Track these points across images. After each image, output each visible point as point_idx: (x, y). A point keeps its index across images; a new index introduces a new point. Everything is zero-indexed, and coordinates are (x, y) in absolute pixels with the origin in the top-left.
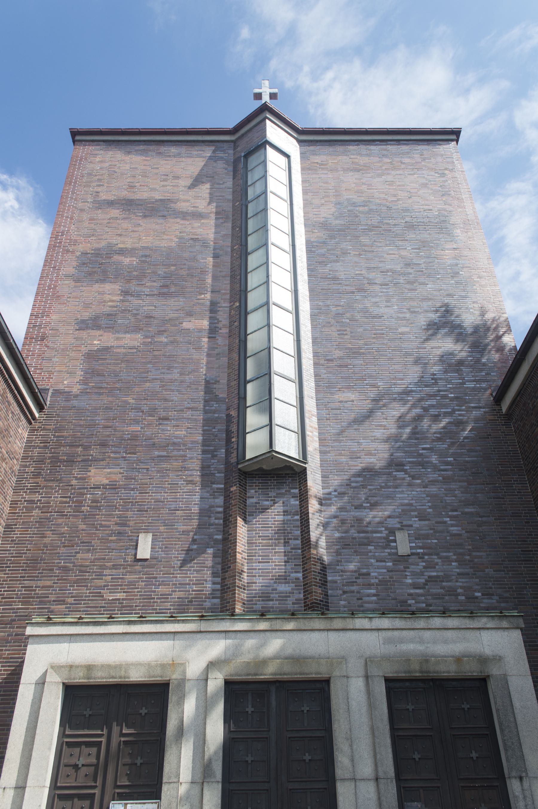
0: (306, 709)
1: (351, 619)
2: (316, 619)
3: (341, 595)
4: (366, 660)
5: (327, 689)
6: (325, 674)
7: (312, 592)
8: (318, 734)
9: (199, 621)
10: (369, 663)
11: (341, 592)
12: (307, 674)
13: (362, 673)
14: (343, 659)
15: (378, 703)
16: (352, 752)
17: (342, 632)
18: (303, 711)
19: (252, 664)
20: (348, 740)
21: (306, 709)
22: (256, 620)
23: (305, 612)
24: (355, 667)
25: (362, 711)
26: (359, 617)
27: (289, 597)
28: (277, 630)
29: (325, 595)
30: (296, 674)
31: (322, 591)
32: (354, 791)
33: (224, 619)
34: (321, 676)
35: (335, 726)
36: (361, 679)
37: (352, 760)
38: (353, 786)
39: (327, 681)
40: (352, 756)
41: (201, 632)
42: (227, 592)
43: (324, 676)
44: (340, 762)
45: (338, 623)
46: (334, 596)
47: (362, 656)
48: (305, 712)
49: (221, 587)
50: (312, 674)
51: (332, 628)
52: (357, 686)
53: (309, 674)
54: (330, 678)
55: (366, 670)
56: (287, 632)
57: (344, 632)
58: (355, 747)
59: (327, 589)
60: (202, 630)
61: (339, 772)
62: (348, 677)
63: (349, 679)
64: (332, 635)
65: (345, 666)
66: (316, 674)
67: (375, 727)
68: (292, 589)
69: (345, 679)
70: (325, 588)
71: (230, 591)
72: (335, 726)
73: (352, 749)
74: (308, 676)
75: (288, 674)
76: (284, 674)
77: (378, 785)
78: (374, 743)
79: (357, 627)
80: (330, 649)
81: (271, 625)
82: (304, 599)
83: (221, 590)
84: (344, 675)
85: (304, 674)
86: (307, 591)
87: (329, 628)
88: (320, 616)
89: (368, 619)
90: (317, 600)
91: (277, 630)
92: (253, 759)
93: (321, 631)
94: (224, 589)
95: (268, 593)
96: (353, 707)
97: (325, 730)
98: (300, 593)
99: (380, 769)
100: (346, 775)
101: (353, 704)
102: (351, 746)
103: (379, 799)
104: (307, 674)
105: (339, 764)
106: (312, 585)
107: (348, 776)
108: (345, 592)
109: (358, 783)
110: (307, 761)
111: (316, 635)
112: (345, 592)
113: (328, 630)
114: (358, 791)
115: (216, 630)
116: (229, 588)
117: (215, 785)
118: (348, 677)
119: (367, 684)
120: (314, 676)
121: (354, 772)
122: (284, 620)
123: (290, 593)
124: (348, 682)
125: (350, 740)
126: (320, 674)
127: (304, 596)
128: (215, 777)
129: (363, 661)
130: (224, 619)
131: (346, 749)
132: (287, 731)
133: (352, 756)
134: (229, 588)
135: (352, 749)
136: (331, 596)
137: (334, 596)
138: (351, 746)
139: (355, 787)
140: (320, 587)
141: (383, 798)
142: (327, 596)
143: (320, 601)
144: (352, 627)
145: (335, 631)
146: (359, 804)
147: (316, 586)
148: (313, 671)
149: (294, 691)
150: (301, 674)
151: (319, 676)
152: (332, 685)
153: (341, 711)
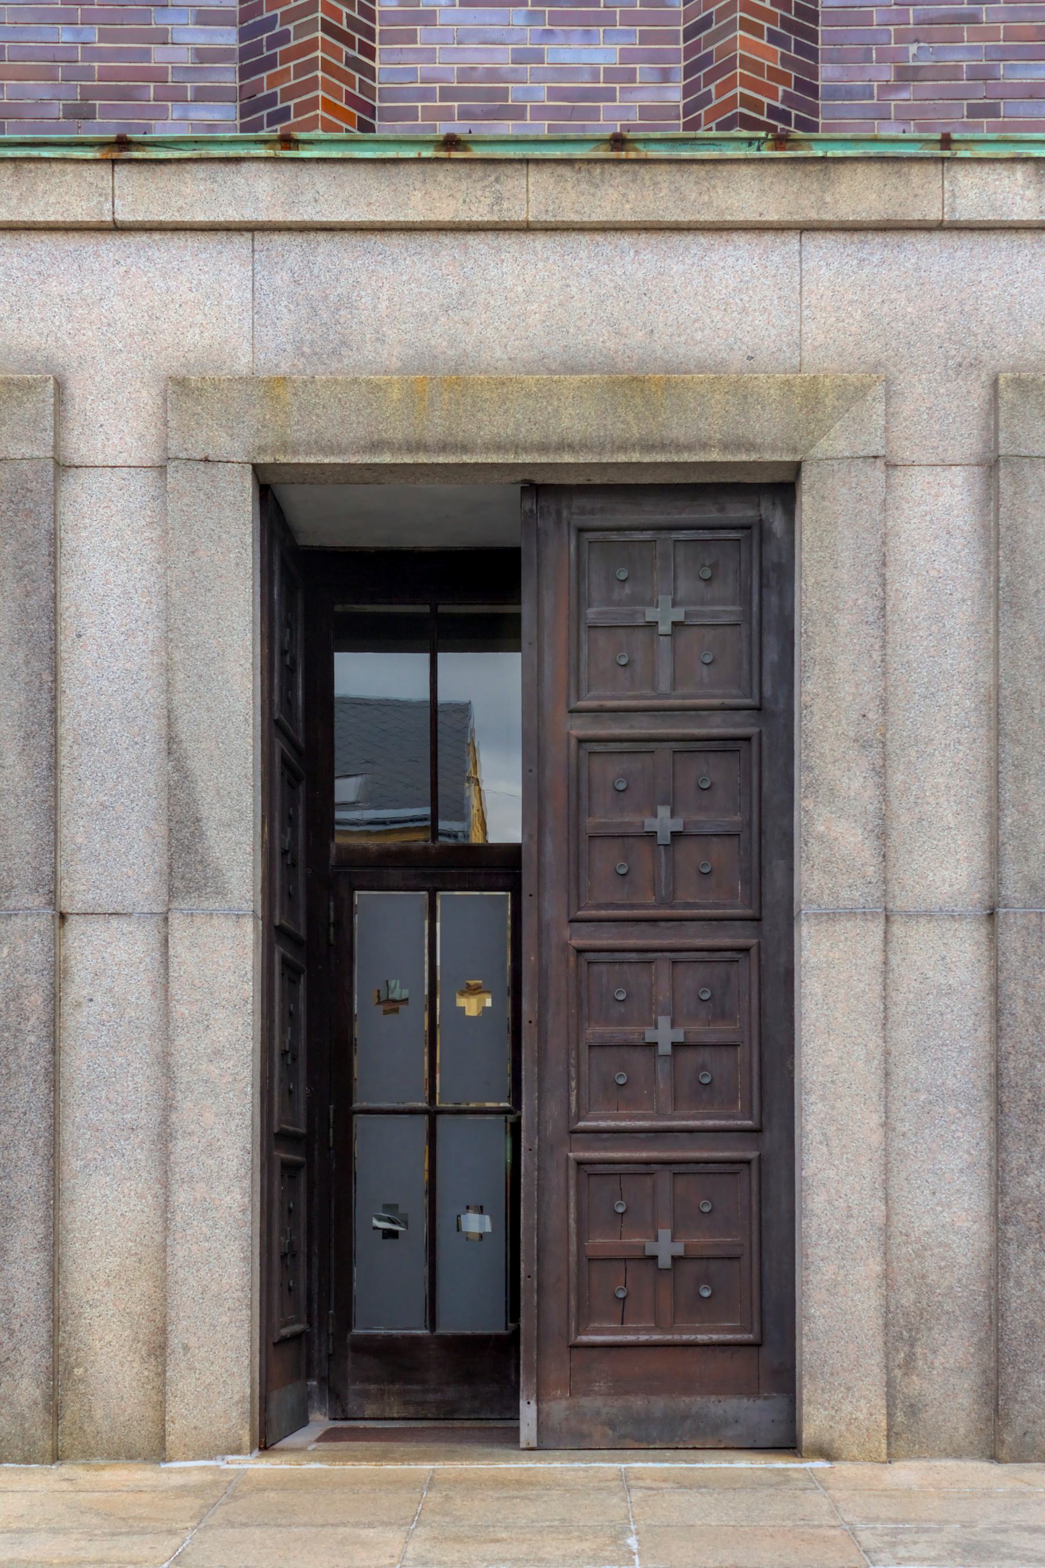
0: (664, 615)
1: (933, 169)
2: (745, 170)
3: (886, 88)
4: (995, 382)
5: (778, 524)
6: (774, 449)
7: (730, 65)
8: (717, 727)
9: (104, 170)
10: (1007, 395)
11: (888, 74)
12: (679, 448)
13: (966, 441)
14: (869, 384)
15: (1032, 585)
16: (885, 799)
17: (878, 239)
18: (653, 625)
19: (395, 394)
20: (865, 745)
21: (664, 615)
22: (414, 169)
23: (691, 134)
24: (940, 417)
25: (949, 623)
26: (980, 161)
27: (609, 95)
28: (527, 228)
29: (800, 84)
30: (623, 448)
31: (785, 60)
32: (879, 957)
33: (238, 160)
34: (753, 457)
35: (809, 686)
36: (959, 476)
37: (882, 835)
38: (877, 939)
39: (782, 488)
40: (883, 818)
41: (117, 228)
42: (270, 63)
43: (768, 457)
44: (821, 838)
45: (860, 194)
46: (850, 94)
47: (976, 364)
48: (665, 628)
49: (243, 36)
50: (705, 446)
51: (828, 217)
52: (938, 506)
53: (689, 448)
54: (797, 468)
55: (992, 430)
56: (585, 239)
57: (892, 238)
58: (898, 779)
59: (813, 54)
60: (124, 216)
61: (812, 881)
62: (891, 466)
63: (899, 473)
64: (825, 257)
65: (881, 407)
66: (725, 447)
67: (1005, 693)
68: (626, 56)
69: (878, 473)
70: (800, 48)
71: (288, 56)
72: (809, 688)
73: (883, 788)
74: (686, 457)
75: (585, 446)
76: (563, 446)
77: (993, 938)
78: (996, 762)
79: (965, 213)
80: (809, 327)
81: (499, 199)
82: (688, 109)
83: (244, 53)
84: (871, 450)
85: (663, 447)
86: (707, 59)
87: (813, 215)
88: (766, 153)
89: (1030, 167)
90: (757, 106)
91: (527, 228)
92: (681, 1039)
93: (768, 238)
94: (256, 49)
95: (493, 74)
96: (906, 605)
97: (759, 709)
98: (665, 76)
99: (1010, 871)
100: (845, 894)
101: (909, 591)
102: (881, 772)
103: (996, 989)
104: (679, 448)
105: (815, 848)
106: (730, 27)
107: (852, 895)
108: (906, 75)
109: (897, 929)
110: (664, 838)
111: (737, 257)
112: (906, 75)
113: (805, 228)
114: (895, 960)
115: (201, 217)
116: (284, 37)
117: (225, 927)
118: (891, 466)
119: (990, 497)
120: (715, 456)
121: (885, 882)
122: (565, 171)
123: (611, 74)
124: (889, 487)
125: (881, 754)
126: (751, 447)
127: (687, 91)
128: (221, 892)
129: (978, 396)
130: (238, 160)
131: (856, 785)
132: (571, 712)
133: (883, 818)
134: (284, 37)
135: (883, 788)
136: (834, 93)
137: (850, 94)
138: (881, 772)
139: (886, 941)
140: (774, 37)
141: (1010, 987)
142: (813, 91)
143: (773, 112)
144: (934, 214)
145: (842, 237)
146: (893, 1011)
147: (756, 30)
148: (704, 435)
149: (614, 536)
150: (650, 447)
151: (744, 458)
152: (806, 501)
153: (844, 622)
